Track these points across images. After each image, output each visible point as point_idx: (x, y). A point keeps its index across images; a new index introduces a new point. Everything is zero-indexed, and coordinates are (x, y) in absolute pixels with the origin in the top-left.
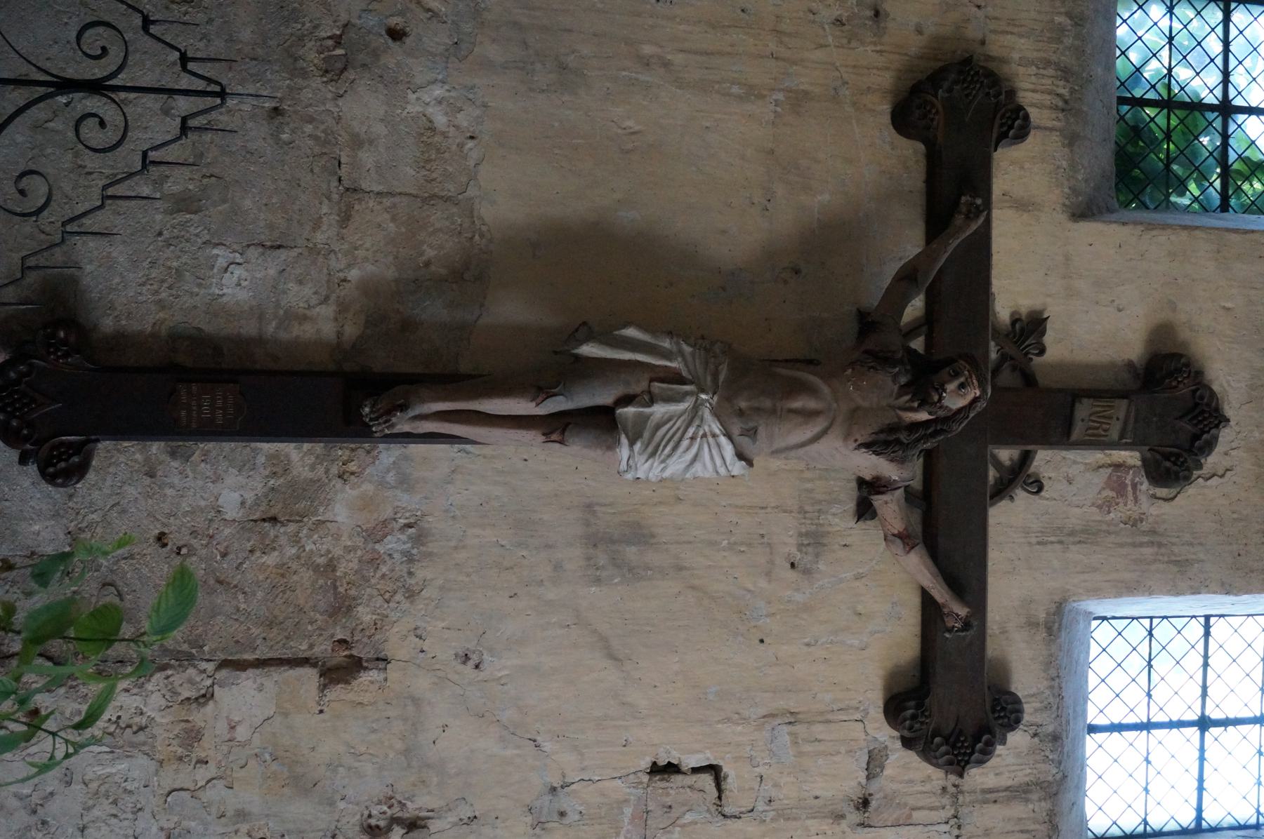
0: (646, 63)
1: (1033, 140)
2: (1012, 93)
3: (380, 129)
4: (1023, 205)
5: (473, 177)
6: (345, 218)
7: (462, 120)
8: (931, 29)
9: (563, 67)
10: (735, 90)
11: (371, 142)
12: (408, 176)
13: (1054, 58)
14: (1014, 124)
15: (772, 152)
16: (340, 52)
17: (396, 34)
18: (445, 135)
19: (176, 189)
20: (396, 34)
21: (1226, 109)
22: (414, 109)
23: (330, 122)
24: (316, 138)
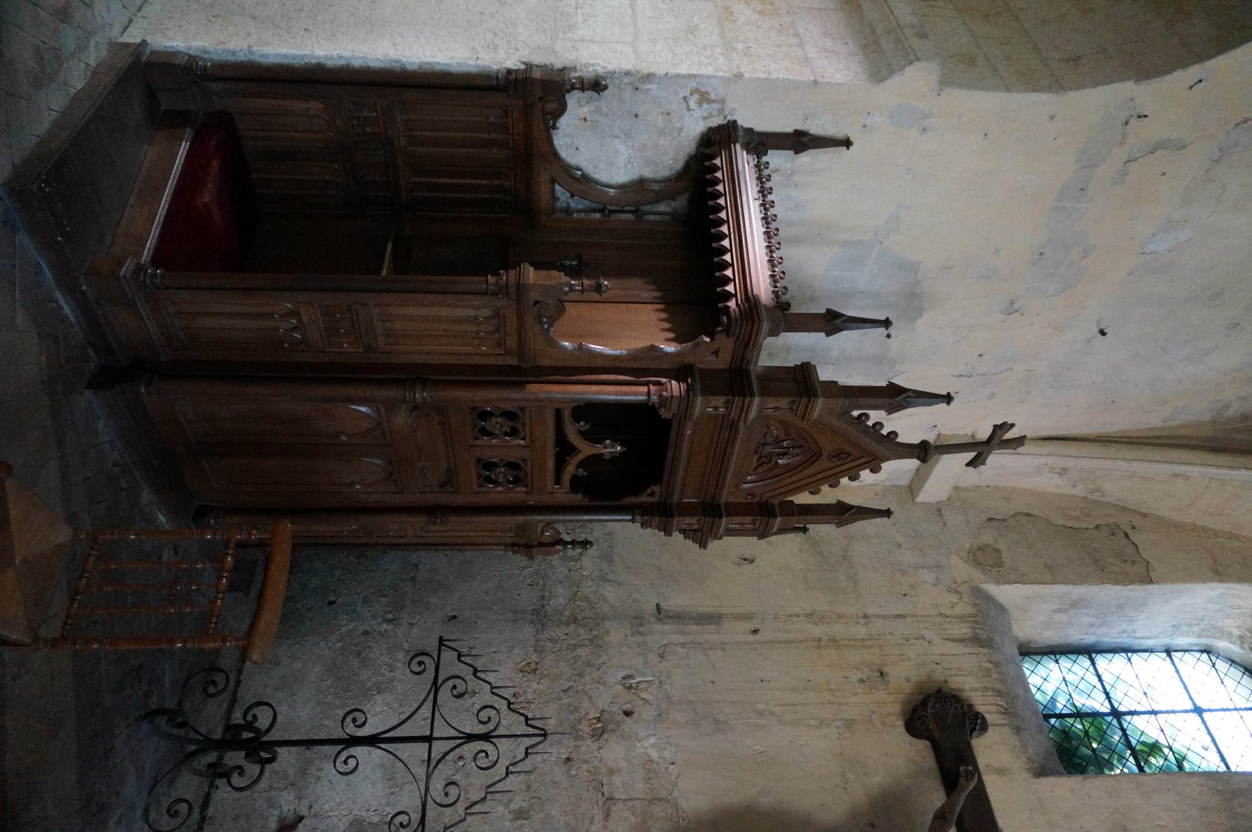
0: (761, 714)
1: (991, 731)
2: (970, 706)
3: (623, 764)
4: (1000, 771)
5: (675, 786)
6: (607, 816)
7: (666, 754)
8: (914, 679)
9: (717, 721)
10: (813, 722)
11: (618, 771)
12: (640, 789)
13: (989, 685)
14: (977, 723)
15: (841, 755)
16: (599, 725)
17: (628, 714)
18: (658, 763)
19: (517, 806)
20: (628, 714)
21: (1116, 713)
22: (640, 751)
23: (596, 762)
24: (589, 771)
